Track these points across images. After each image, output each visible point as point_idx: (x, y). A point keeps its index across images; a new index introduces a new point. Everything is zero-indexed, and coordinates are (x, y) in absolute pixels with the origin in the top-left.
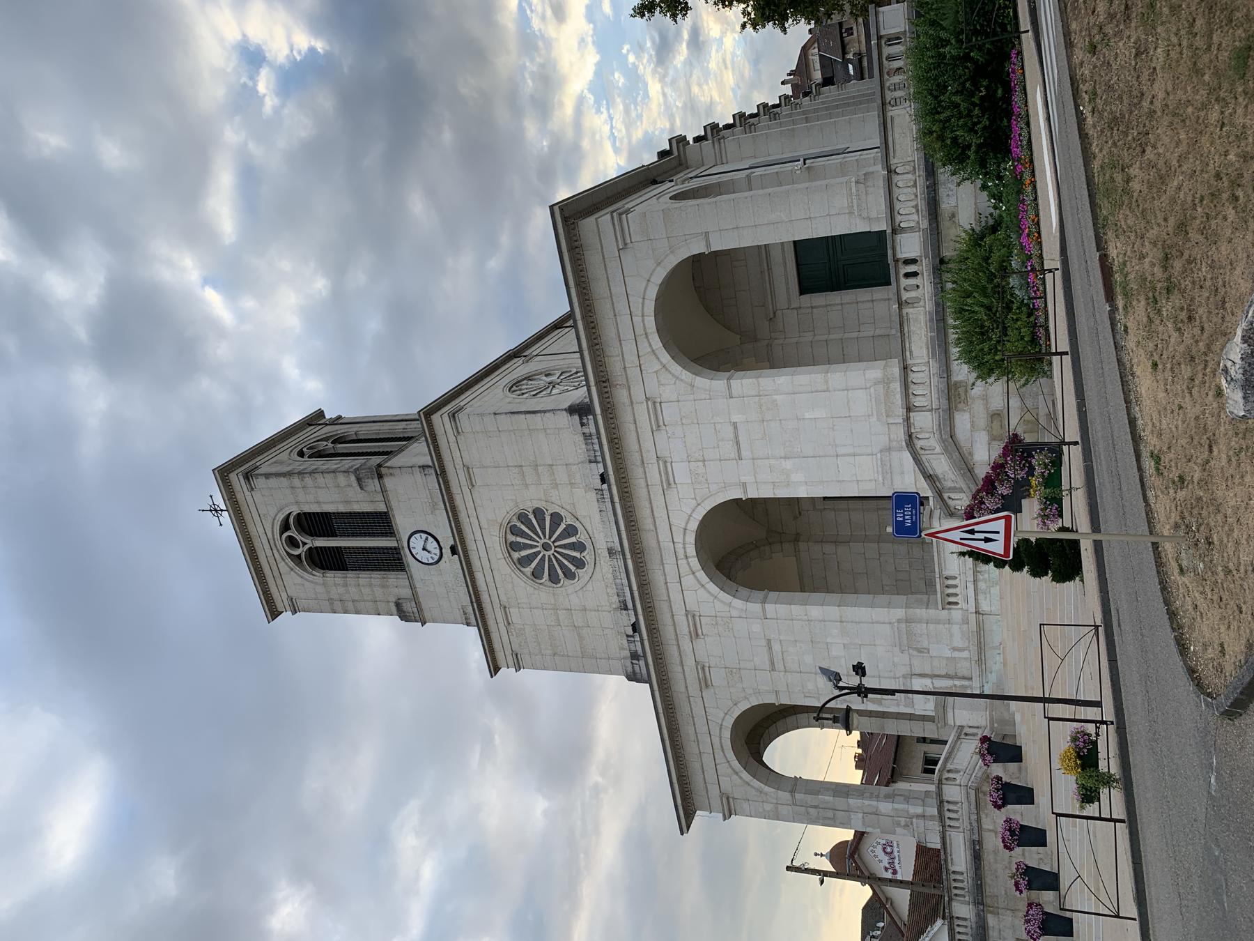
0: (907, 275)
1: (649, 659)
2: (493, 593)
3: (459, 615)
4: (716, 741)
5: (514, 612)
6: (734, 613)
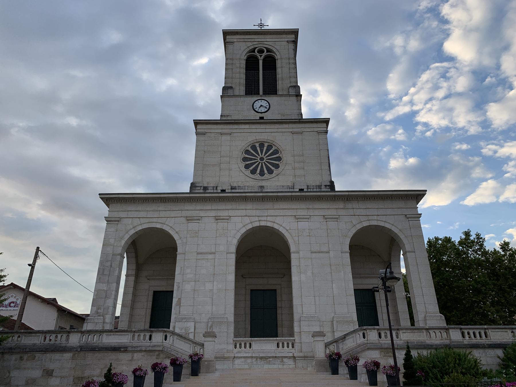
0: (474, 334)
1: (201, 195)
2: (238, 131)
3: (226, 113)
4: (155, 220)
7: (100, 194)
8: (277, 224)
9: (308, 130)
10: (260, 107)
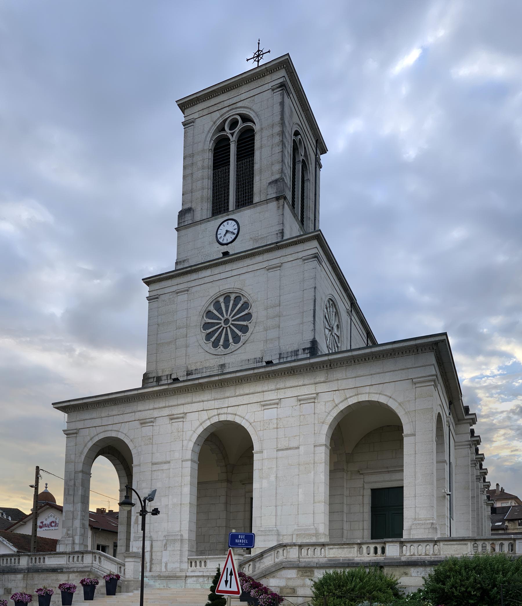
0: (376, 549)
1: (159, 386)
3: (183, 257)
5: (183, 297)
7: (53, 404)
8: (239, 416)
9: (290, 258)
10: (225, 235)
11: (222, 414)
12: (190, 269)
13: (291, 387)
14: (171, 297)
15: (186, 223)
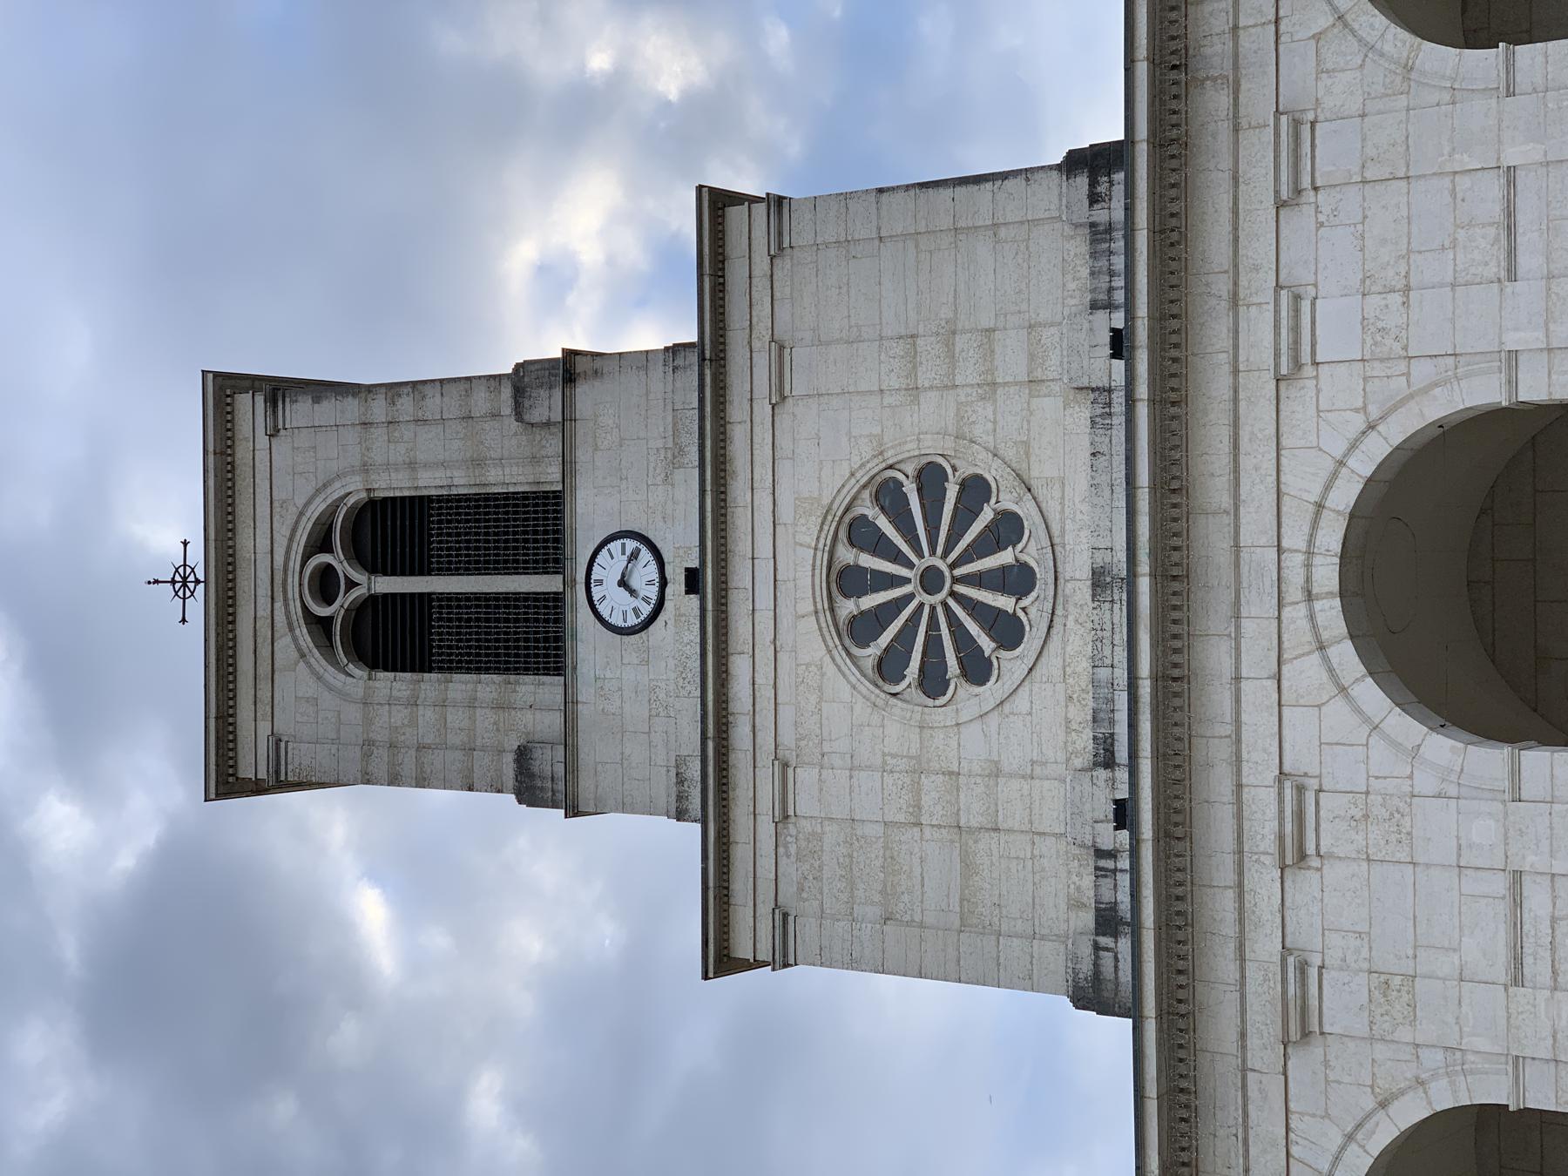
3: (663, 787)
5: (805, 777)
6: (1425, 782)
8: (1328, 487)
10: (632, 592)
11: (1308, 580)
12: (710, 744)
13: (1236, 239)
14: (793, 849)
15: (560, 769)
